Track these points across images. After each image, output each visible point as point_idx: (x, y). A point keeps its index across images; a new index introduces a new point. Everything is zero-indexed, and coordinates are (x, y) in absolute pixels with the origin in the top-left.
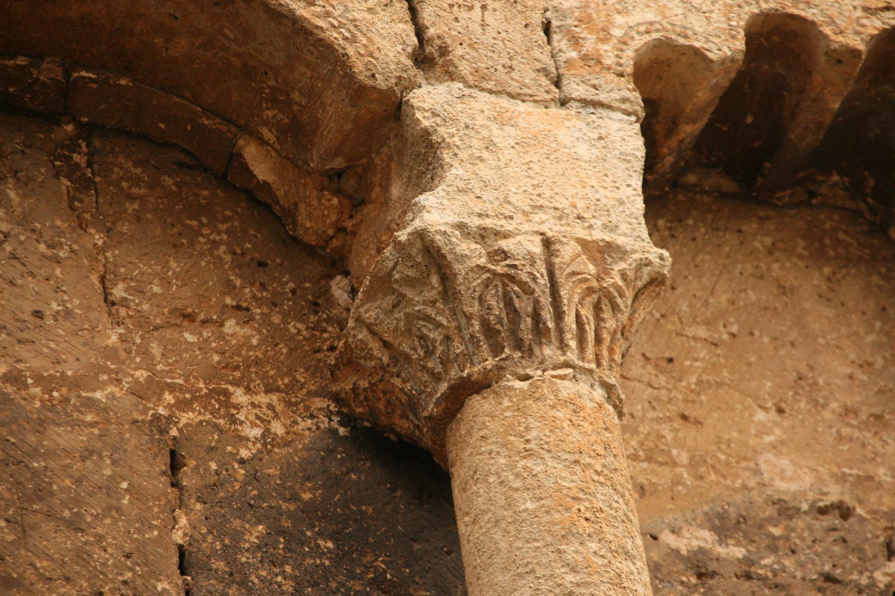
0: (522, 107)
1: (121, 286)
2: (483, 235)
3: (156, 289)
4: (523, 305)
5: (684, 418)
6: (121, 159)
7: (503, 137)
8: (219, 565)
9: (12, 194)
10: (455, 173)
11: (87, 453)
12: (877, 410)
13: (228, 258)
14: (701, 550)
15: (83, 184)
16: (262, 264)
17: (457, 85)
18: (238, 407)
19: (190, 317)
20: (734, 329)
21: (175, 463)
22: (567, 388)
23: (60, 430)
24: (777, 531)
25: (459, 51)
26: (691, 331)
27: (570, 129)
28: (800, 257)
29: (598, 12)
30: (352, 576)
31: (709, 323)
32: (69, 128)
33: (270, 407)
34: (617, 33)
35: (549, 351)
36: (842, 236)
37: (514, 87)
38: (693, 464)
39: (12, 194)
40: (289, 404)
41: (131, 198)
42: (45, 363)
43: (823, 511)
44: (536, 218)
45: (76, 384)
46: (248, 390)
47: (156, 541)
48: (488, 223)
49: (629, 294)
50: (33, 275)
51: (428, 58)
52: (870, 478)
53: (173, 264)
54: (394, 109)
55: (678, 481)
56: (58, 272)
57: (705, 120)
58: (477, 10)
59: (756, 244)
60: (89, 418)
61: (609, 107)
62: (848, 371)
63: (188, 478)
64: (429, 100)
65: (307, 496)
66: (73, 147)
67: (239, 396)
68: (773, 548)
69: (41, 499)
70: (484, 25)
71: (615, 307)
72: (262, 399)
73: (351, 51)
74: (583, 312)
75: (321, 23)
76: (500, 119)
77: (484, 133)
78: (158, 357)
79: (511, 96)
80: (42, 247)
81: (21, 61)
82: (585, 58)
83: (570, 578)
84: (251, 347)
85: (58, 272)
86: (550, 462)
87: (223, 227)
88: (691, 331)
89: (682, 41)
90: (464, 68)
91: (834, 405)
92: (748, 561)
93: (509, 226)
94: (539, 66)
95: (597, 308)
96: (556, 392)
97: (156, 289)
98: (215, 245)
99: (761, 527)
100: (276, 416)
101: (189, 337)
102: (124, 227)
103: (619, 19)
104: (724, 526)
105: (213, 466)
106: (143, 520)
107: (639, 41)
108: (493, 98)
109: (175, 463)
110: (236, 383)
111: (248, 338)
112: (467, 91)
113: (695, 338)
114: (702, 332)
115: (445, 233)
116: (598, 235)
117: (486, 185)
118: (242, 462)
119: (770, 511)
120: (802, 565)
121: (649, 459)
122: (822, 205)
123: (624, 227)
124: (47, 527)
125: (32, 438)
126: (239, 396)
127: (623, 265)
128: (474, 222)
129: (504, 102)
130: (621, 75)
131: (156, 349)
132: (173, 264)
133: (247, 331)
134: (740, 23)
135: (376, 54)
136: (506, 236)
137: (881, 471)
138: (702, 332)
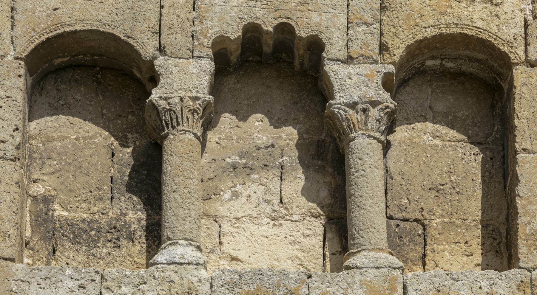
0: (181, 60)
1: (105, 110)
2: (166, 99)
3: (113, 110)
4: (174, 116)
5: (237, 126)
6: (109, 75)
7: (175, 70)
8: (119, 181)
9: (82, 89)
10: (162, 81)
11: (92, 156)
12: (285, 118)
13: (131, 99)
14: (235, 162)
15: (99, 83)
16: (140, 99)
17: (167, 57)
18: (128, 139)
19: (121, 116)
20: (254, 100)
21: (113, 155)
22: (182, 137)
23: (86, 150)
24: (254, 155)
25: (168, 47)
26: (243, 102)
27: (193, 66)
28: (274, 77)
29: (205, 30)
30: (150, 180)
31: (248, 99)
32: (98, 68)
33: (137, 138)
34: (209, 35)
35: (180, 128)
36: (286, 70)
37: (180, 56)
38: (237, 139)
39: (82, 89)
40: (141, 136)
41: (110, 85)
42: (85, 133)
43: (268, 147)
44: (179, 92)
45: (91, 138)
46: (132, 134)
47: (105, 177)
48: (167, 95)
49: (201, 109)
50: (85, 110)
51: (161, 50)
52: (281, 137)
53: (118, 102)
54: (151, 64)
55: (233, 144)
56: (91, 108)
57: (240, 49)
58: (175, 34)
59: (264, 75)
60: (93, 146)
61: (204, 58)
62: (281, 108)
63: (115, 159)
64: (160, 61)
65: (142, 160)
66: (98, 74)
67: (129, 136)
68: (253, 159)
69: (80, 169)
70: (176, 39)
71: (198, 114)
72: (135, 136)
73: (141, 52)
74: (188, 116)
75: (135, 45)
76: (176, 65)
77: (171, 69)
78: (111, 128)
79: (179, 58)
80: (88, 102)
81: (81, 56)
82: (200, 44)
83: (175, 187)
84: (134, 122)
85: (91, 108)
86: (175, 157)
87: (131, 90)
88: (243, 102)
89: (225, 35)
90: (168, 52)
91: (275, 118)
92: (246, 163)
93: (172, 95)
94: (188, 48)
95: (193, 114)
96: (179, 138)
97: (113, 110)
98: (128, 95)
99: (251, 154)
100: (138, 140)
101: (119, 122)
102: (107, 94)
103: (210, 31)
104: (241, 156)
105: (121, 155)
106: (103, 171)
107: (214, 37)
108: (174, 59)
109: (113, 155)
110: (129, 132)
111: (133, 120)
112: (168, 58)
113: (244, 104)
114: (246, 102)
115: (156, 100)
116: (195, 94)
117: (168, 84)
118: (128, 153)
119: (254, 149)
120: (259, 163)
121: (226, 139)
122: (283, 61)
123: (201, 91)
124: (81, 175)
125: (80, 153)
126: (129, 136)
127: (200, 102)
128: (164, 96)
129: (177, 60)
130: (208, 47)
131: (111, 125)
132: (118, 102)
133: (134, 118)
134: (241, 27)
135: (147, 51)
136: (172, 98)
137: (283, 135)
138: (246, 102)
